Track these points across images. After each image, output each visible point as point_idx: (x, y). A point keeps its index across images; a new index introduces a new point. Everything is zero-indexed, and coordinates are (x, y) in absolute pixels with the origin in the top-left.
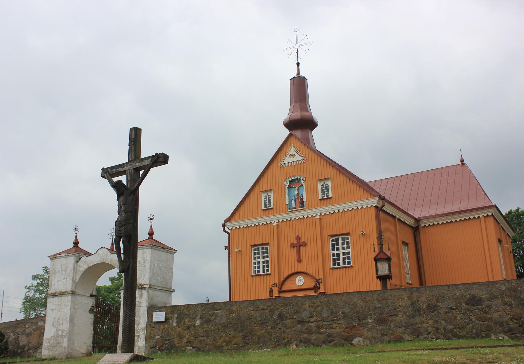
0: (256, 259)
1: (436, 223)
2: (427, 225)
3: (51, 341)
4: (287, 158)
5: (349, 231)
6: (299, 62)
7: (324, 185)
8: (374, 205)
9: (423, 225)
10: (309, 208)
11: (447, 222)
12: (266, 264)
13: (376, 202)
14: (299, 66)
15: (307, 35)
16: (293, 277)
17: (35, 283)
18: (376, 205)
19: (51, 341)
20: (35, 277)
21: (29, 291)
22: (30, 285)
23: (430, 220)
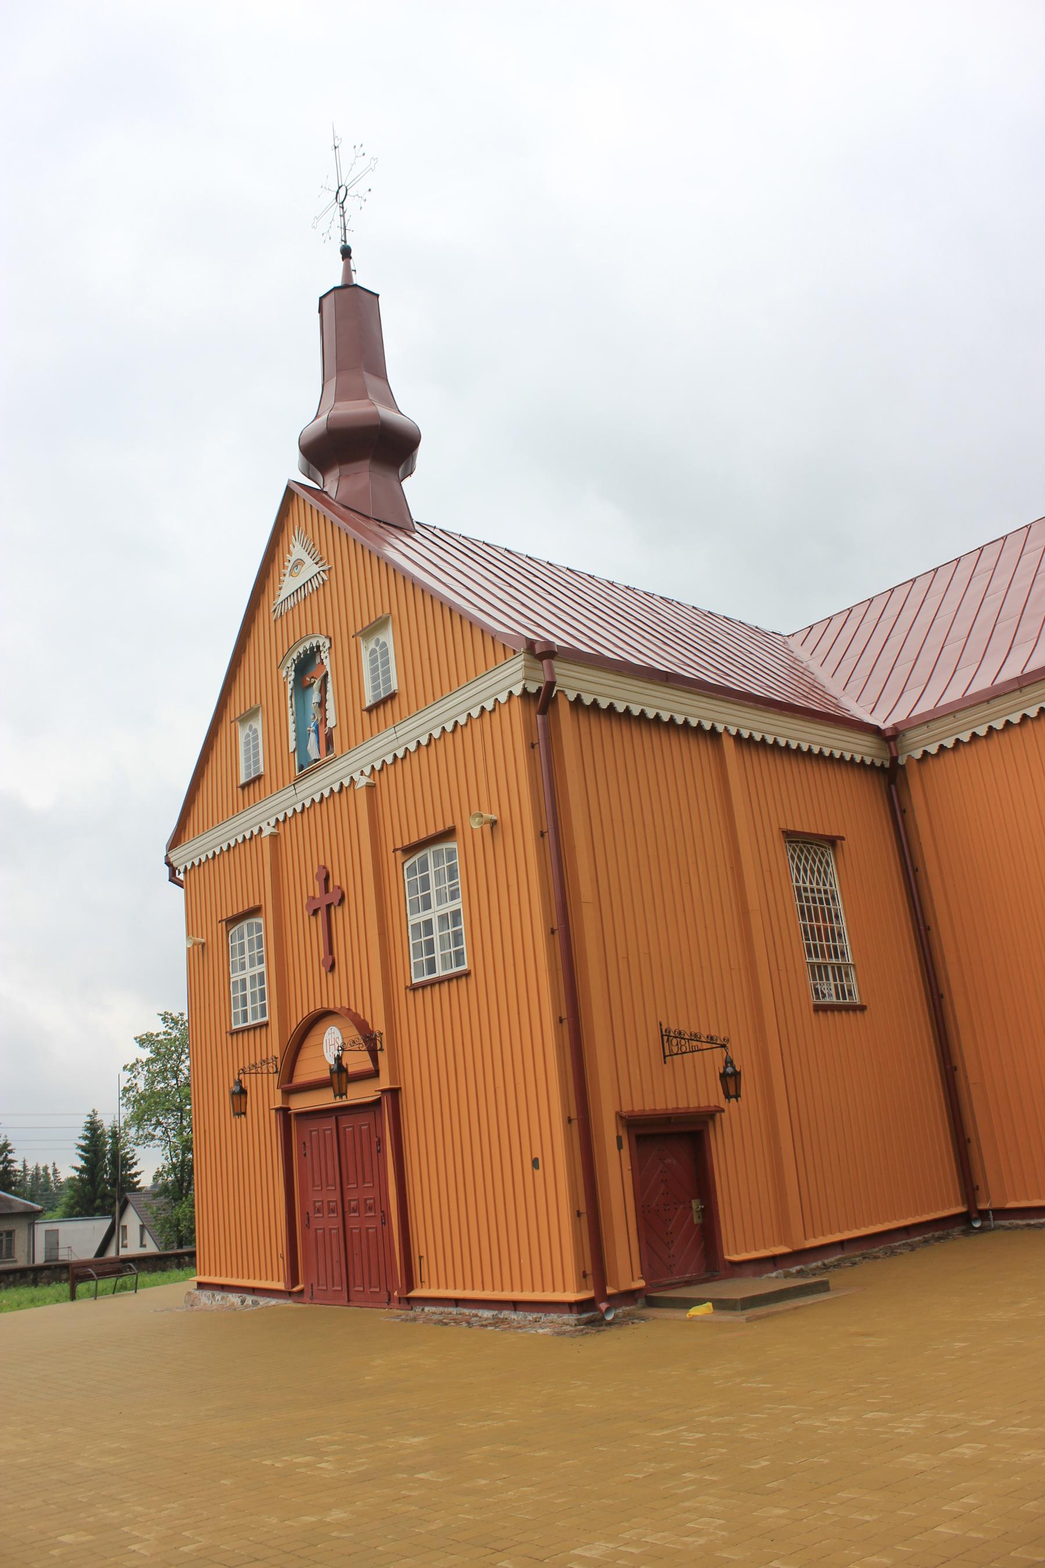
0: (259, 974)
1: (965, 737)
2: (933, 749)
3: (186, 1207)
4: (287, 579)
5: (453, 823)
6: (348, 243)
7: (378, 649)
8: (517, 691)
9: (918, 754)
10: (351, 747)
11: (1008, 723)
12: (831, 946)
13: (520, 675)
14: (351, 258)
15: (361, 146)
16: (311, 1041)
17: (146, 1054)
18: (525, 689)
19: (186, 1207)
20: (143, 1041)
21: (135, 1077)
22: (133, 1062)
23: (938, 727)
